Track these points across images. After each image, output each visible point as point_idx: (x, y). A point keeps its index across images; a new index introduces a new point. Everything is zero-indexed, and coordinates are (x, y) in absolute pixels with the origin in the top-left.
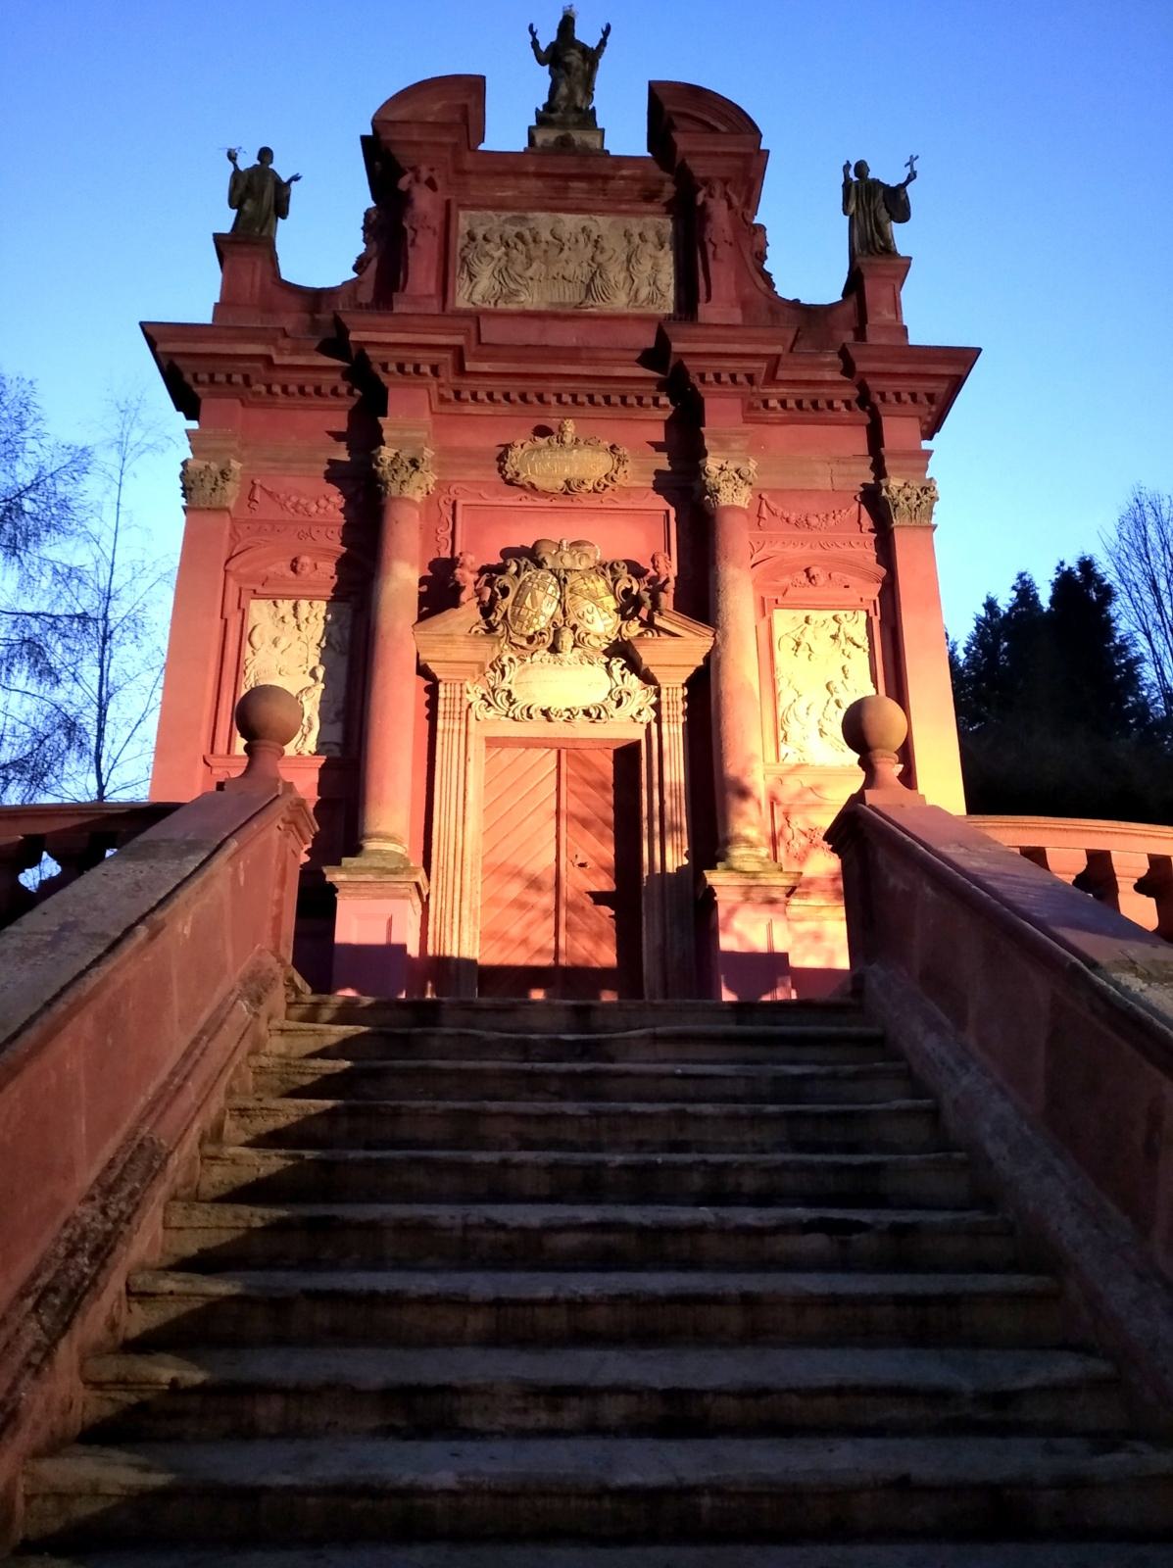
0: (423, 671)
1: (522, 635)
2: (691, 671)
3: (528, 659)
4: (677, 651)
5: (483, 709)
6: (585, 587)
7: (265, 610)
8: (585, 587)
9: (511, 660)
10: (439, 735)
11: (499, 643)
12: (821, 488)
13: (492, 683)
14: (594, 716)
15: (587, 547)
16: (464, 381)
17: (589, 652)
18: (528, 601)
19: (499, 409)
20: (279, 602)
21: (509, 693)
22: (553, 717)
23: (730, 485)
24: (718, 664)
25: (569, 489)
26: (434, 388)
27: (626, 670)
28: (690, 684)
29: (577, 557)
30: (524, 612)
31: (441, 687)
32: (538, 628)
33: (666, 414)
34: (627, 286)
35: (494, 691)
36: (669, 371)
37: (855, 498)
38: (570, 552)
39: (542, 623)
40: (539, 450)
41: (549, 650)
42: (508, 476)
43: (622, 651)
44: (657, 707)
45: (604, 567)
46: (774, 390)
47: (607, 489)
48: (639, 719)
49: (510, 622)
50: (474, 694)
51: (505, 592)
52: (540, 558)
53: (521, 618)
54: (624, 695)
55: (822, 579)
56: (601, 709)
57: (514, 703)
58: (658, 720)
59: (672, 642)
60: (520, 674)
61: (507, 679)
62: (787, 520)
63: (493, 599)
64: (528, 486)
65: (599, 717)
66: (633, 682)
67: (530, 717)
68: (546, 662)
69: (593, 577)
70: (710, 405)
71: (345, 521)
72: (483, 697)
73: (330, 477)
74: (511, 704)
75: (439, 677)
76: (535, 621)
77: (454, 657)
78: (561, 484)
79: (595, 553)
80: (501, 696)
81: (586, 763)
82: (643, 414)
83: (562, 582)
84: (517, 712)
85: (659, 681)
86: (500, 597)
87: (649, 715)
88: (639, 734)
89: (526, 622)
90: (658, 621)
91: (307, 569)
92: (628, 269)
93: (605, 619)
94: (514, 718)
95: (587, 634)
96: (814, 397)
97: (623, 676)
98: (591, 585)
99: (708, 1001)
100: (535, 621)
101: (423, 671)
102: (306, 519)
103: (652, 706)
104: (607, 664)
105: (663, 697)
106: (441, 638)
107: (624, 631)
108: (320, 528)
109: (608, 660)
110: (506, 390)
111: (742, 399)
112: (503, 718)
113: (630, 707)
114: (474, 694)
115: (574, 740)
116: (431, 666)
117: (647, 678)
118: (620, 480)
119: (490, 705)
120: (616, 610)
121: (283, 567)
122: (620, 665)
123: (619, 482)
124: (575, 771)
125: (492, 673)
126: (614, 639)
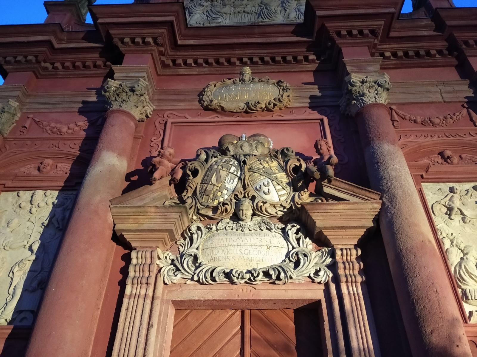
0: (118, 238)
1: (208, 207)
2: (362, 232)
3: (214, 228)
4: (348, 215)
5: (171, 274)
6: (261, 167)
7: (10, 199)
8: (261, 167)
9: (199, 228)
10: (125, 301)
11: (187, 215)
12: (434, 100)
13: (181, 249)
14: (274, 277)
15: (262, 137)
16: (179, 53)
17: (266, 219)
18: (214, 180)
19: (203, 70)
20: (21, 193)
21: (196, 258)
22: (235, 279)
23: (372, 91)
24: (391, 224)
25: (249, 110)
26: (156, 54)
27: (300, 234)
28: (361, 244)
29: (254, 145)
30: (209, 187)
31: (134, 254)
32: (221, 200)
33: (313, 67)
34: (283, 13)
35: (182, 256)
36: (315, 35)
37: (463, 106)
38: (248, 142)
39: (226, 195)
40: (226, 87)
41: (232, 218)
42: (205, 104)
43: (296, 218)
44: (333, 267)
45: (277, 152)
46: (388, 46)
47: (276, 108)
48: (317, 280)
49: (199, 196)
50: (164, 258)
51: (195, 173)
52: (224, 148)
53: (207, 193)
54: (301, 256)
55: (456, 160)
56: (280, 269)
57: (199, 266)
58: (336, 279)
59: (341, 206)
60: (206, 241)
61: (195, 245)
62: (415, 122)
63: (185, 177)
64: (220, 110)
65: (278, 278)
66: (308, 244)
67: (214, 280)
68: (229, 230)
69: (267, 159)
70: (344, 50)
71: (85, 136)
72: (173, 263)
73: (81, 112)
74: (197, 268)
75: (133, 245)
76: (219, 194)
77: (145, 227)
78: (242, 105)
79: (269, 143)
80: (188, 261)
81: (269, 324)
82: (298, 68)
83: (242, 164)
84: (202, 275)
85: (333, 242)
86: (191, 178)
87: (325, 275)
88: (318, 294)
89: (211, 196)
90: (327, 190)
91: (48, 168)
92: (283, 6)
93: (279, 190)
94: (198, 281)
95: (264, 203)
96: (416, 49)
97: (298, 240)
98: (266, 165)
99: (175, 21)
100: (219, 194)
101: (118, 238)
102: (60, 136)
103: (329, 267)
104: (283, 230)
105: (338, 257)
106: (134, 210)
107: (297, 199)
108: (65, 142)
109: (283, 226)
110: (206, 57)
111: (368, 46)
112: (189, 282)
113: (308, 268)
114: (164, 258)
115: (255, 302)
116: (126, 235)
117: (321, 241)
118: (285, 101)
119: (178, 269)
120: (288, 184)
121: (31, 169)
122: (294, 230)
123: (285, 102)
124: (258, 332)
125: (182, 241)
126: (288, 207)
